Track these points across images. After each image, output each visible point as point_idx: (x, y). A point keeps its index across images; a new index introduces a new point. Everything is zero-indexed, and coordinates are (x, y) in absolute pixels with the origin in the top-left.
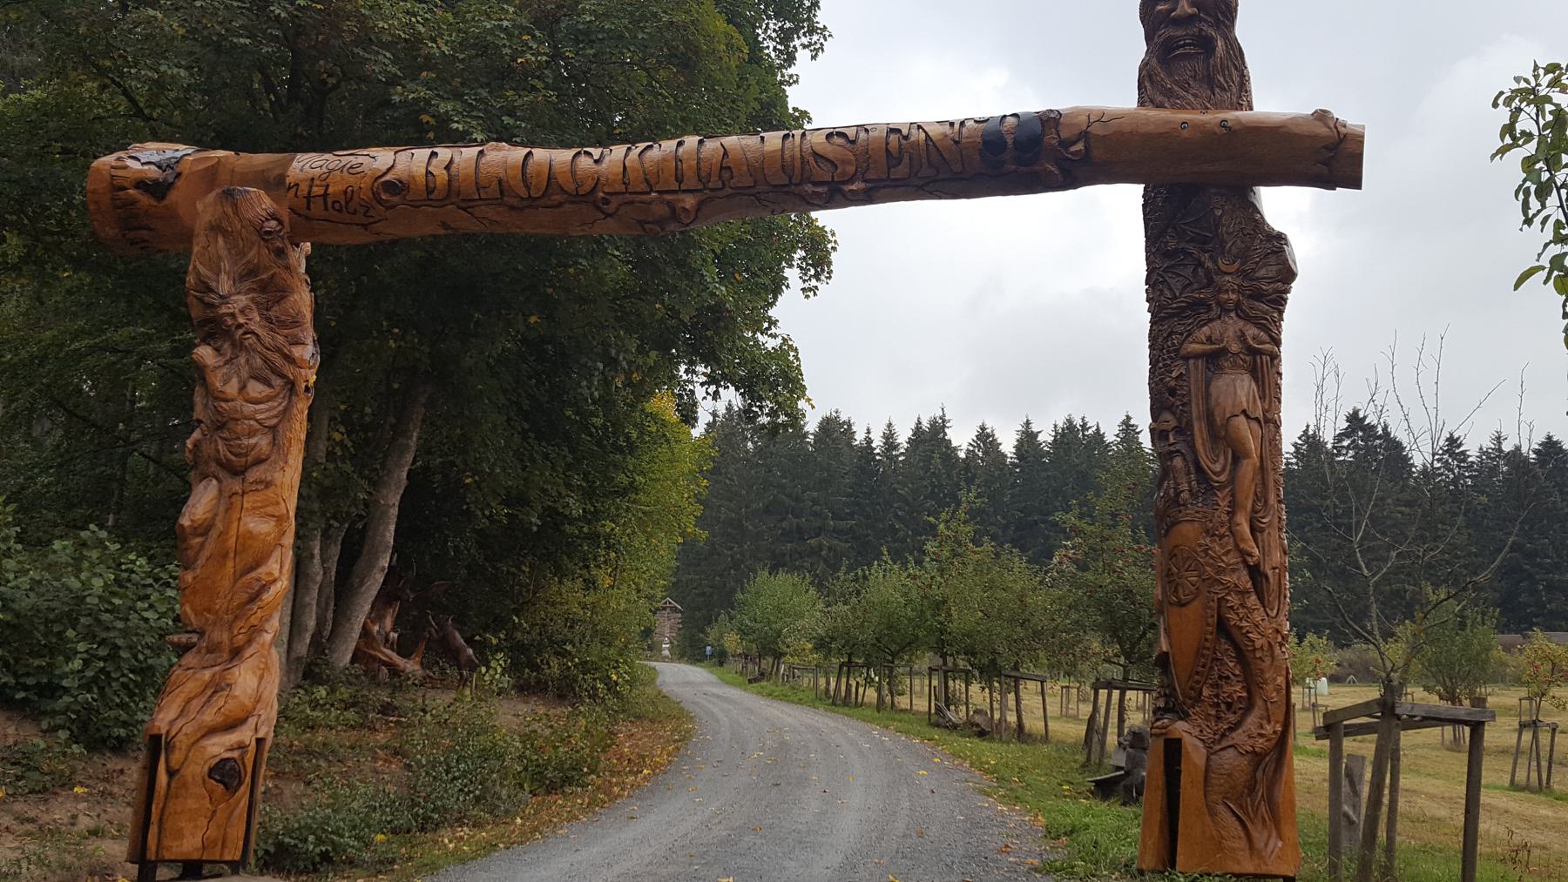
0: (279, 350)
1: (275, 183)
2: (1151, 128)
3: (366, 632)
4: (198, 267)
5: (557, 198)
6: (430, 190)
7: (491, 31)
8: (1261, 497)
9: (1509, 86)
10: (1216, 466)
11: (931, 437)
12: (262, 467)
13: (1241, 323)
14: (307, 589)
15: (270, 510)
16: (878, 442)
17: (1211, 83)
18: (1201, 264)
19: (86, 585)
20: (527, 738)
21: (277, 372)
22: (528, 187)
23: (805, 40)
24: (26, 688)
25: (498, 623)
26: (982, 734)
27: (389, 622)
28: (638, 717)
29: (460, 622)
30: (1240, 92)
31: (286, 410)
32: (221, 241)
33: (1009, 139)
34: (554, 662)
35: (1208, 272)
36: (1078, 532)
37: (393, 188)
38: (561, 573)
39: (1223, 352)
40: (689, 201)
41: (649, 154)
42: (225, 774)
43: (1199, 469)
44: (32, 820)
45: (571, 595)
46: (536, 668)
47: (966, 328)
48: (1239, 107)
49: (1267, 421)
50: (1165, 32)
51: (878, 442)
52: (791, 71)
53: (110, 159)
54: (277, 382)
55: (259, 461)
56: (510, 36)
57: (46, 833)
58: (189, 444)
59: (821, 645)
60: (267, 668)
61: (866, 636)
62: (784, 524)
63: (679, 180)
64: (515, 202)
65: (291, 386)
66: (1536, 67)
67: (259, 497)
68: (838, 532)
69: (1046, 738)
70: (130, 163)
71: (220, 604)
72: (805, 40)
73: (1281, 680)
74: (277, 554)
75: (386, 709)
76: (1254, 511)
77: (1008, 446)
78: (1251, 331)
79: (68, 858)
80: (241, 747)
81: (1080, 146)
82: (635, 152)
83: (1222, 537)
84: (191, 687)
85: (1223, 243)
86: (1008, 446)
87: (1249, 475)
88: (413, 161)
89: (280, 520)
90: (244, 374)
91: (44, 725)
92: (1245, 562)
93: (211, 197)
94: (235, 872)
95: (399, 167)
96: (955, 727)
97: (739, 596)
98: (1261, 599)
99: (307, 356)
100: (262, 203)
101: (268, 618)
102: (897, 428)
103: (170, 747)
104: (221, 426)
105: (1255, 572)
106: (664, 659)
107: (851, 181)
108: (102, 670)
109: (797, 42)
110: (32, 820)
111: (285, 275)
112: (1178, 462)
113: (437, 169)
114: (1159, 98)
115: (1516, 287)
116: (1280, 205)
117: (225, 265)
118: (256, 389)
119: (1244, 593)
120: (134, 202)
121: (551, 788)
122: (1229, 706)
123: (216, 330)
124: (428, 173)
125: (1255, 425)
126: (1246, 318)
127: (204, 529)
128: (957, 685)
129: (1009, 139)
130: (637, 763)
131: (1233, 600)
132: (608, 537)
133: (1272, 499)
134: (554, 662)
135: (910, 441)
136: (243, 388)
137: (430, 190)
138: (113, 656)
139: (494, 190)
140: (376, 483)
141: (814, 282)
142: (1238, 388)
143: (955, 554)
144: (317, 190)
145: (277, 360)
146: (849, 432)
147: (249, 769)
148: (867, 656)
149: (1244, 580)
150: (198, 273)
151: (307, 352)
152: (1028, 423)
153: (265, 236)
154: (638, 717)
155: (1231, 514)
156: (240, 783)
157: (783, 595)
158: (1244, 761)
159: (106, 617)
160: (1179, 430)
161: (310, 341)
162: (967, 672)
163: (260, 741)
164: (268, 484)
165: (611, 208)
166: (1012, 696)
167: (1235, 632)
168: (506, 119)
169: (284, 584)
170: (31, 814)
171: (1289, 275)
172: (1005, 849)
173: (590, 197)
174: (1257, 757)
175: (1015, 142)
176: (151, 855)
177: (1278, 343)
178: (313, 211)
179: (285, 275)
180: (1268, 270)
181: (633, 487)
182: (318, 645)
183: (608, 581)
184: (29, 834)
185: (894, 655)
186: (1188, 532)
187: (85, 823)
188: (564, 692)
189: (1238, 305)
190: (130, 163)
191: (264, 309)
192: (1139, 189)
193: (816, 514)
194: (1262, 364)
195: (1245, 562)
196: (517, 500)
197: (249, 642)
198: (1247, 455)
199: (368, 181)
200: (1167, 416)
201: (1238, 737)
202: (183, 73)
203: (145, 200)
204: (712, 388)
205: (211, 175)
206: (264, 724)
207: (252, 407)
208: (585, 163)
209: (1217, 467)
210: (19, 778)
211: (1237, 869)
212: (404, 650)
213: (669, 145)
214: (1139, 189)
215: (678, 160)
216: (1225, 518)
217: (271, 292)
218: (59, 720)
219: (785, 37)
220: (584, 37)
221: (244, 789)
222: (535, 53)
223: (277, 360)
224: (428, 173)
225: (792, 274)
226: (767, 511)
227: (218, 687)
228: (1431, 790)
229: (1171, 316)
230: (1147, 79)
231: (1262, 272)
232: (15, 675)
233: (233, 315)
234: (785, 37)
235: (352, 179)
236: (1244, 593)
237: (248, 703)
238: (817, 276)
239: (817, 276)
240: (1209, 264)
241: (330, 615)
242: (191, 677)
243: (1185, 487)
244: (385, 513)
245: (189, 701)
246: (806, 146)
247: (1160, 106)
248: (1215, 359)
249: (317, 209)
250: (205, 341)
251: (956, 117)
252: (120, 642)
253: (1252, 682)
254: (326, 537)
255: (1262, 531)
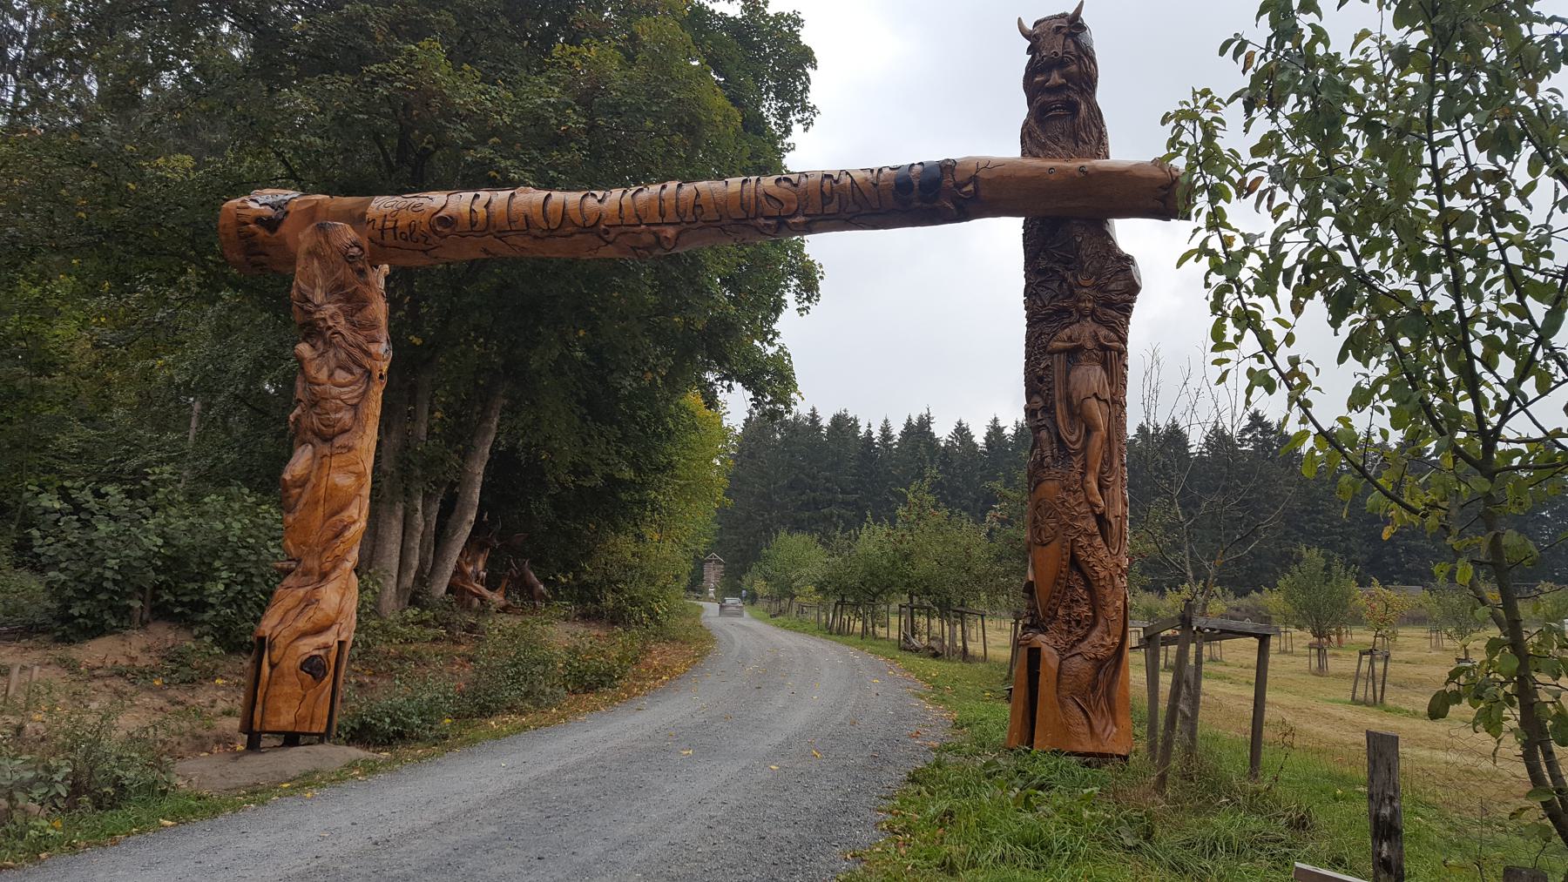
0: (359, 347)
1: (357, 219)
2: (1026, 172)
3: (459, 571)
4: (299, 282)
5: (570, 229)
6: (473, 223)
7: (540, 107)
8: (1108, 461)
9: (1173, 108)
10: (1072, 437)
11: (919, 431)
12: (346, 436)
13: (1095, 326)
14: (412, 536)
15: (351, 468)
16: (876, 434)
17: (1075, 137)
18: (1064, 279)
19: (228, 527)
20: (575, 651)
21: (357, 363)
22: (548, 222)
23: (799, 117)
24: (183, 604)
25: (568, 566)
26: (936, 655)
27: (481, 564)
28: (672, 640)
29: (538, 563)
30: (1099, 143)
31: (365, 392)
32: (316, 262)
33: (916, 183)
34: (609, 596)
35: (1070, 285)
36: (1005, 497)
37: (445, 222)
38: (617, 530)
39: (1080, 348)
40: (670, 232)
41: (640, 195)
42: (313, 667)
43: (1060, 440)
44: (182, 703)
45: (624, 545)
46: (597, 602)
47: (910, 338)
48: (1098, 156)
49: (1114, 402)
50: (1041, 98)
51: (876, 434)
52: (787, 141)
53: (236, 202)
54: (358, 371)
55: (344, 431)
56: (556, 109)
57: (187, 711)
58: (292, 418)
59: (821, 588)
60: (347, 588)
61: (854, 582)
62: (804, 497)
63: (662, 215)
64: (538, 233)
65: (369, 374)
66: (1194, 93)
67: (343, 458)
68: (845, 504)
69: (985, 659)
70: (251, 204)
71: (313, 539)
72: (799, 117)
73: (1119, 603)
74: (357, 502)
75: (471, 628)
76: (1102, 472)
77: (979, 439)
78: (1103, 332)
79: (199, 731)
80: (326, 647)
81: (970, 187)
82: (630, 193)
83: (1075, 492)
84: (289, 602)
85: (1082, 263)
86: (979, 439)
87: (1099, 444)
88: (460, 202)
89: (359, 476)
90: (332, 364)
91: (196, 632)
92: (1093, 511)
93: (309, 230)
94: (321, 741)
95: (450, 206)
96: (917, 650)
97: (765, 551)
98: (1105, 540)
99: (382, 352)
100: (347, 234)
101: (349, 551)
102: (892, 424)
103: (271, 647)
104: (314, 404)
105: (1101, 520)
106: (710, 600)
107: (794, 215)
108: (240, 592)
109: (793, 118)
110: (182, 703)
111: (366, 290)
112: (1044, 434)
113: (479, 207)
114: (1035, 150)
115: (1179, 266)
116: (1133, 235)
117: (319, 281)
118: (341, 376)
119: (1092, 535)
120: (254, 234)
121: (589, 689)
122: (1078, 623)
123: (311, 331)
124: (472, 210)
125: (1103, 404)
126: (1101, 322)
127: (302, 483)
128: (922, 621)
129: (916, 183)
130: (657, 673)
131: (1083, 541)
132: (653, 502)
133: (1116, 463)
134: (609, 596)
135: (902, 434)
136: (331, 375)
137: (473, 223)
138: (248, 582)
139: (521, 225)
140: (465, 455)
141: (806, 304)
142: (1091, 376)
143: (920, 517)
144: (389, 224)
145: (357, 353)
146: (856, 427)
147: (333, 664)
148: (854, 598)
149: (1092, 525)
150: (299, 289)
151: (382, 348)
152: (996, 420)
153: (349, 259)
154: (672, 640)
155: (1083, 474)
156: (325, 674)
157: (804, 555)
158: (1089, 665)
159: (242, 551)
160: (1045, 409)
161: (384, 340)
162: (929, 609)
163: (341, 643)
164: (350, 449)
165: (611, 237)
166: (959, 627)
167: (1084, 565)
168: (551, 173)
169: (362, 524)
170: (181, 698)
171: (1134, 289)
172: (917, 735)
173: (594, 227)
174: (1099, 663)
175: (920, 185)
176: (256, 728)
177: (1125, 342)
178: (386, 240)
179: (366, 290)
180: (1118, 285)
181: (671, 465)
182: (421, 579)
183: (657, 537)
184: (178, 713)
185: (875, 595)
186: (1050, 487)
187: (222, 705)
188: (617, 618)
189: (1093, 312)
190: (251, 204)
191: (349, 316)
192: (1019, 222)
193: (827, 489)
194: (1112, 358)
195: (1093, 511)
196: (579, 470)
197: (334, 568)
198: (1097, 428)
199: (427, 217)
200: (1037, 398)
201: (1084, 647)
202: (318, 141)
203: (262, 232)
204: (726, 383)
205: (312, 213)
206: (346, 630)
207: (338, 390)
208: (591, 201)
209: (1074, 438)
210: (174, 672)
211: (1080, 749)
212: (491, 584)
213: (655, 189)
214: (1019, 222)
215: (661, 199)
216: (1078, 477)
217: (355, 303)
218: (206, 628)
219: (784, 114)
220: (615, 109)
221: (328, 679)
222: (575, 121)
223: (357, 353)
224: (472, 210)
225: (789, 297)
226: (791, 486)
227: (309, 602)
228: (1286, 703)
229: (1041, 320)
230: (1027, 135)
231: (1113, 286)
232: (175, 595)
233: (324, 320)
234: (784, 114)
235: (414, 216)
236: (1092, 535)
237: (332, 614)
238: (808, 299)
239: (808, 299)
240: (1071, 280)
241: (431, 557)
242: (289, 595)
243: (1048, 453)
244: (472, 480)
245: (286, 613)
246: (760, 189)
247: (1037, 156)
248: (1074, 354)
249: (389, 238)
250: (305, 340)
251: (876, 165)
252: (253, 571)
253: (1096, 604)
254: (428, 497)
255: (1108, 487)
